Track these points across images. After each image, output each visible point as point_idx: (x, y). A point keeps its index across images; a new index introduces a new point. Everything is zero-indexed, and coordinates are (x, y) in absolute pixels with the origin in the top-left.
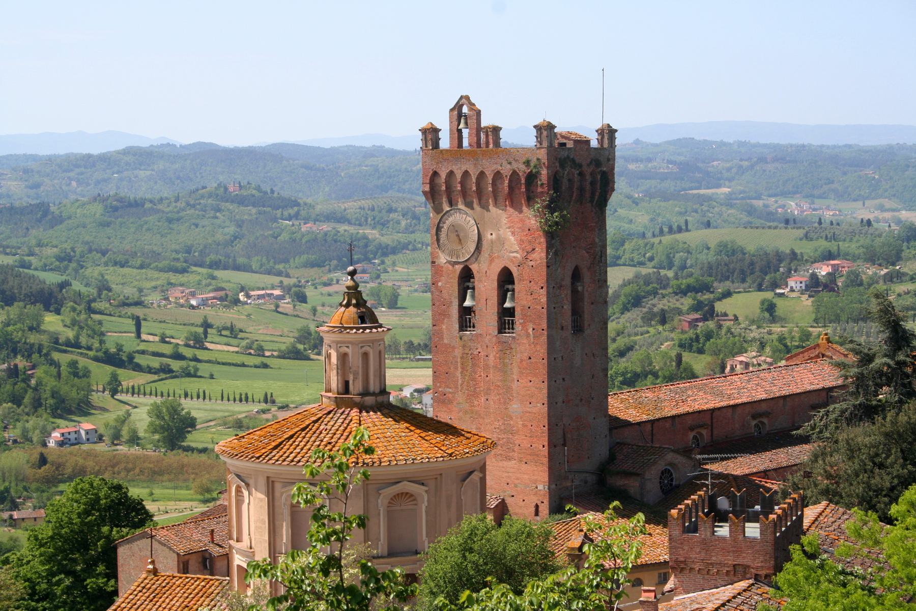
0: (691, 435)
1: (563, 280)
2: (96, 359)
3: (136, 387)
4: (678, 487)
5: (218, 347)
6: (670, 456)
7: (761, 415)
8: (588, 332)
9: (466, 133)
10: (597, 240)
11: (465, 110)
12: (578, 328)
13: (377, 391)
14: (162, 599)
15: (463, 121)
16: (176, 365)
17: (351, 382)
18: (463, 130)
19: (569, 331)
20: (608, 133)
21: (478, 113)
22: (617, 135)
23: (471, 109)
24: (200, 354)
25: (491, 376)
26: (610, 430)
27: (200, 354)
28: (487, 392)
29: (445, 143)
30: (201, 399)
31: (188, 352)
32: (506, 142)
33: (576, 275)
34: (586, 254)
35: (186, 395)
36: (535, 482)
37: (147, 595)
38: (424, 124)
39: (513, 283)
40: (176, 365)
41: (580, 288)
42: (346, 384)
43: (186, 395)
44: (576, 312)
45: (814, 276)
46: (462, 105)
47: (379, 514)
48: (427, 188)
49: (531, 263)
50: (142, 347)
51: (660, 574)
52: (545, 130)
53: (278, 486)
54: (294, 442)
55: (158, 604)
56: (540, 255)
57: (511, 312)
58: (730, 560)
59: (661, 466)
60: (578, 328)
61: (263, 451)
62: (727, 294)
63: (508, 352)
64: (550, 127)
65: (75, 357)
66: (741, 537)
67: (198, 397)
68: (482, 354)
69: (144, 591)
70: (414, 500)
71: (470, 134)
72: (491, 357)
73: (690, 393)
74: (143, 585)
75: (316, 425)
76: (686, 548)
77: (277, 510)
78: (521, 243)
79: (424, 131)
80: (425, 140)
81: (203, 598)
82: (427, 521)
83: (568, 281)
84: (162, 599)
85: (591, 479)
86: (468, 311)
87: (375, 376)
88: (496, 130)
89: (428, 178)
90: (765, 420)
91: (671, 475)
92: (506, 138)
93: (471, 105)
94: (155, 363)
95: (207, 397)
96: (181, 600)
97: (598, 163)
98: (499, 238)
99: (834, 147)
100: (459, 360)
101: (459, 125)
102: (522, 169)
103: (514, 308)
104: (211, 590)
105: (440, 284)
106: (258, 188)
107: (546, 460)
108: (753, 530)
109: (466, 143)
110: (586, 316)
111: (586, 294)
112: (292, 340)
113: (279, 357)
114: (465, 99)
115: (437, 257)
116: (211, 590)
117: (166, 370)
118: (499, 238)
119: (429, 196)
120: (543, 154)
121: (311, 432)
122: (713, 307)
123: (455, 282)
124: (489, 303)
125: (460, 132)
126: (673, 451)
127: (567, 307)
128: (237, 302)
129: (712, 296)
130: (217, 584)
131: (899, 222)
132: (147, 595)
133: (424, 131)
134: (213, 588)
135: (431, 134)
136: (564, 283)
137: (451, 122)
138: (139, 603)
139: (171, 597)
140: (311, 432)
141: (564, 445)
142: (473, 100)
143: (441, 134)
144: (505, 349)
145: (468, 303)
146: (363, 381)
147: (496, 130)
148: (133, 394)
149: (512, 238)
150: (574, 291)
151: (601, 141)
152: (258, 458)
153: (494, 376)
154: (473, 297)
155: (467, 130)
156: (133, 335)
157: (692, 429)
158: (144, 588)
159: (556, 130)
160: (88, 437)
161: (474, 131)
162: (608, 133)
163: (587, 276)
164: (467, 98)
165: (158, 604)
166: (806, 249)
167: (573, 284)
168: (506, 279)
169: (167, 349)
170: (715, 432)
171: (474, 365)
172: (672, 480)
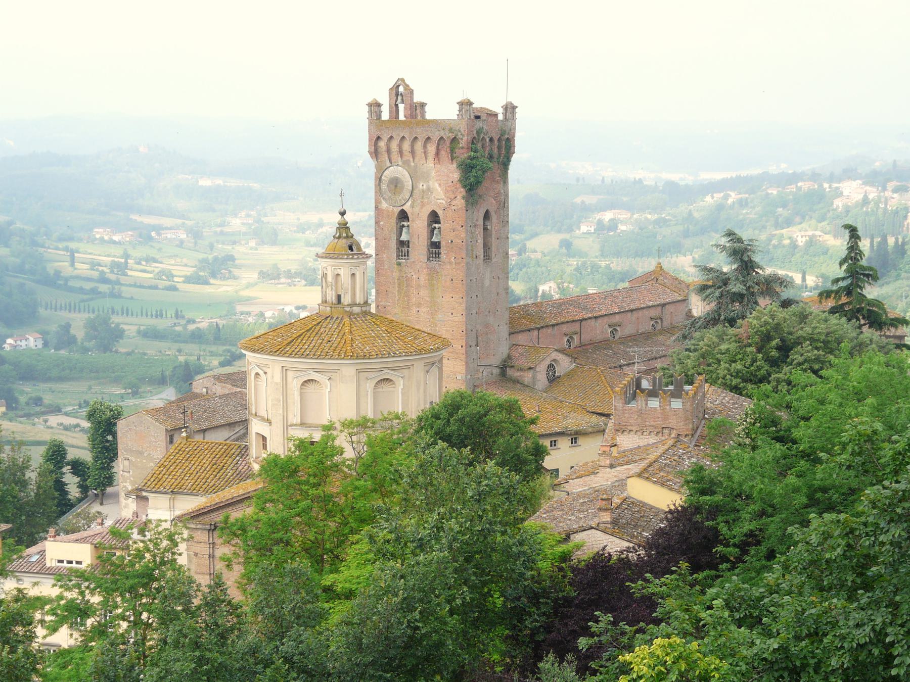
1: (477, 220)
2: (38, 282)
3: (73, 305)
4: (559, 377)
6: (555, 355)
9: (401, 107)
10: (502, 191)
11: (401, 89)
12: (487, 257)
13: (362, 302)
14: (195, 459)
15: (400, 98)
16: (104, 288)
17: (342, 296)
18: (400, 105)
21: (412, 92)
22: (517, 110)
23: (405, 89)
25: (421, 293)
26: (509, 334)
28: (419, 305)
29: (385, 116)
30: (120, 315)
31: (113, 277)
33: (487, 216)
34: (494, 202)
35: (113, 312)
36: (455, 373)
37: (183, 456)
38: (370, 100)
39: (439, 222)
41: (489, 227)
42: (339, 297)
43: (113, 312)
44: (486, 247)
45: (600, 222)
46: (399, 86)
47: (367, 395)
48: (373, 150)
49: (454, 208)
50: (76, 272)
51: (551, 442)
52: (465, 104)
54: (302, 340)
55: (193, 462)
56: (460, 202)
57: (436, 245)
58: (660, 423)
59: (548, 362)
60: (487, 257)
61: (279, 347)
62: (535, 235)
63: (435, 275)
64: (470, 104)
65: (22, 281)
66: (668, 408)
67: (123, 313)
68: (414, 276)
69: (181, 453)
70: (394, 384)
71: (405, 108)
72: (422, 278)
73: (563, 307)
74: (179, 448)
75: (318, 328)
76: (627, 415)
77: (289, 391)
78: (446, 192)
79: (370, 105)
80: (370, 112)
81: (226, 458)
84: (195, 459)
85: (496, 371)
86: (402, 244)
87: (360, 291)
88: (423, 105)
89: (373, 141)
90: (618, 328)
91: (554, 368)
92: (431, 114)
93: (407, 86)
95: (130, 313)
96: (210, 459)
97: (503, 133)
100: (396, 281)
101: (396, 101)
102: (448, 136)
103: (439, 243)
104: (232, 452)
105: (382, 223)
107: (463, 357)
108: (676, 404)
109: (402, 117)
110: (494, 249)
111: (494, 232)
112: (195, 269)
113: (184, 282)
115: (380, 202)
116: (232, 452)
118: (429, 189)
119: (374, 155)
120: (463, 127)
121: (314, 333)
122: (525, 245)
123: (394, 221)
124: (420, 239)
125: (397, 106)
126: (556, 350)
127: (480, 241)
128: (150, 238)
129: (523, 237)
130: (236, 447)
132: (183, 456)
133: (370, 105)
134: (234, 451)
136: (478, 223)
137: (390, 99)
138: (178, 461)
139: (202, 457)
140: (314, 333)
141: (477, 345)
142: (407, 82)
143: (383, 108)
144: (433, 275)
145: (404, 237)
146: (352, 296)
147: (423, 105)
148: (70, 311)
149: (439, 189)
150: (485, 229)
151: (505, 114)
152: (276, 352)
153: (424, 293)
154: (408, 232)
155: (403, 105)
156: (66, 264)
158: (180, 450)
159: (474, 106)
160: (36, 344)
161: (408, 106)
164: (403, 80)
165: (193, 462)
168: (434, 218)
169: (95, 274)
170: (583, 337)
171: (408, 285)
172: (555, 372)
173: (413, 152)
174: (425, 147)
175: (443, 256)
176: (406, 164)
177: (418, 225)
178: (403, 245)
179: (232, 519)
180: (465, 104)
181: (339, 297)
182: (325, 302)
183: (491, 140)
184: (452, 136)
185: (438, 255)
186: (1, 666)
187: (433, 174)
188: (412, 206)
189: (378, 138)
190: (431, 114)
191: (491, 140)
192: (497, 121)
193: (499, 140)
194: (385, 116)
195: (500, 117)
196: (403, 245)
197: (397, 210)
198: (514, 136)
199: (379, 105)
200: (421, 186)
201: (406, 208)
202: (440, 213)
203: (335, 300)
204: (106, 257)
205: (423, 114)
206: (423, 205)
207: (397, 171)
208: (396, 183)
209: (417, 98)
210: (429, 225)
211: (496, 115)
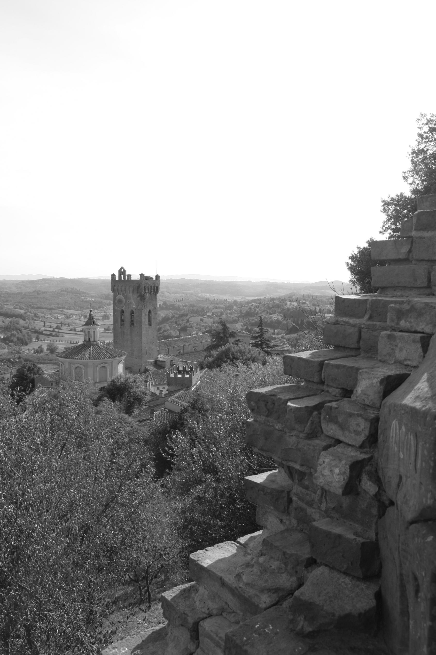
0: (178, 352)
5: (64, 329)
7: (195, 347)
8: (152, 326)
11: (122, 270)
19: (147, 326)
20: (157, 277)
24: (60, 331)
27: (60, 331)
29: (117, 279)
32: (162, 280)
33: (150, 312)
38: (112, 274)
40: (54, 334)
42: (89, 339)
44: (150, 321)
52: (142, 275)
53: (71, 365)
82: (370, 293)
83: (147, 313)
94: (48, 333)
98: (130, 302)
99: (167, 280)
106: (76, 289)
114: (122, 268)
117: (51, 335)
131: (233, 299)
135: (113, 276)
143: (116, 276)
145: (123, 318)
150: (149, 316)
157: (178, 350)
162: (157, 277)
163: (152, 312)
166: (211, 306)
167: (149, 314)
168: (132, 312)
173: (125, 290)
174: (129, 289)
175: (135, 325)
176: (123, 295)
177: (127, 315)
178: (123, 321)
179: (254, 329)
180: (142, 275)
181: (89, 339)
182: (85, 340)
183: (151, 287)
184: (137, 285)
185: (124, 324)
186: (2, 441)
187: (132, 298)
188: (125, 308)
189: (115, 286)
190: (133, 278)
191: (151, 287)
192: (153, 280)
193: (154, 287)
194: (117, 279)
195: (154, 279)
196: (123, 321)
197: (120, 309)
198: (159, 285)
199: (115, 275)
200: (128, 302)
201: (123, 308)
202: (134, 310)
203: (88, 340)
204: (276, 318)
205: (131, 278)
206: (129, 308)
207: (120, 297)
208: (120, 301)
209: (127, 273)
210: (131, 314)
211: (153, 279)
